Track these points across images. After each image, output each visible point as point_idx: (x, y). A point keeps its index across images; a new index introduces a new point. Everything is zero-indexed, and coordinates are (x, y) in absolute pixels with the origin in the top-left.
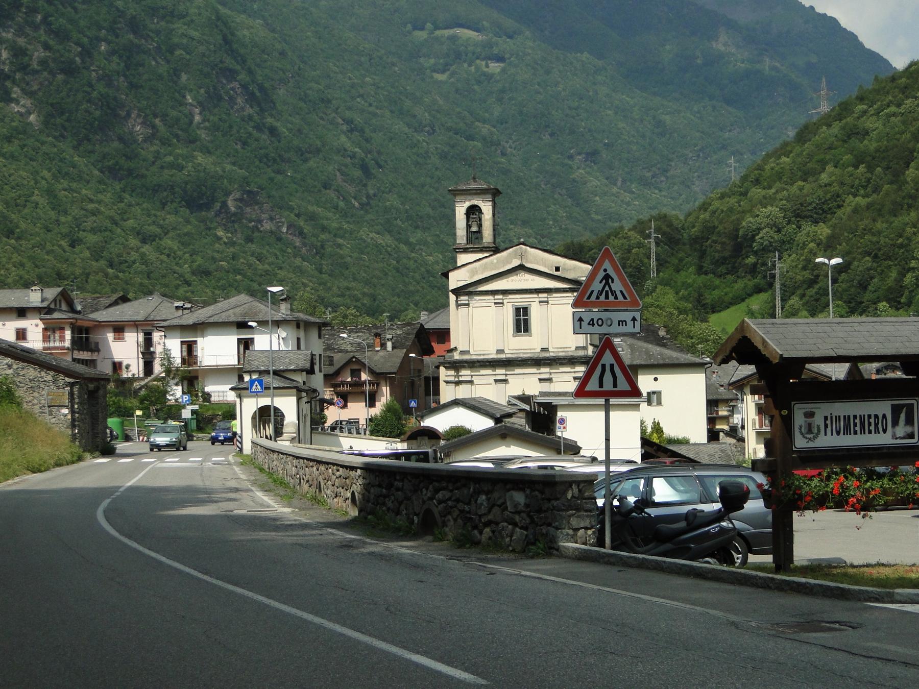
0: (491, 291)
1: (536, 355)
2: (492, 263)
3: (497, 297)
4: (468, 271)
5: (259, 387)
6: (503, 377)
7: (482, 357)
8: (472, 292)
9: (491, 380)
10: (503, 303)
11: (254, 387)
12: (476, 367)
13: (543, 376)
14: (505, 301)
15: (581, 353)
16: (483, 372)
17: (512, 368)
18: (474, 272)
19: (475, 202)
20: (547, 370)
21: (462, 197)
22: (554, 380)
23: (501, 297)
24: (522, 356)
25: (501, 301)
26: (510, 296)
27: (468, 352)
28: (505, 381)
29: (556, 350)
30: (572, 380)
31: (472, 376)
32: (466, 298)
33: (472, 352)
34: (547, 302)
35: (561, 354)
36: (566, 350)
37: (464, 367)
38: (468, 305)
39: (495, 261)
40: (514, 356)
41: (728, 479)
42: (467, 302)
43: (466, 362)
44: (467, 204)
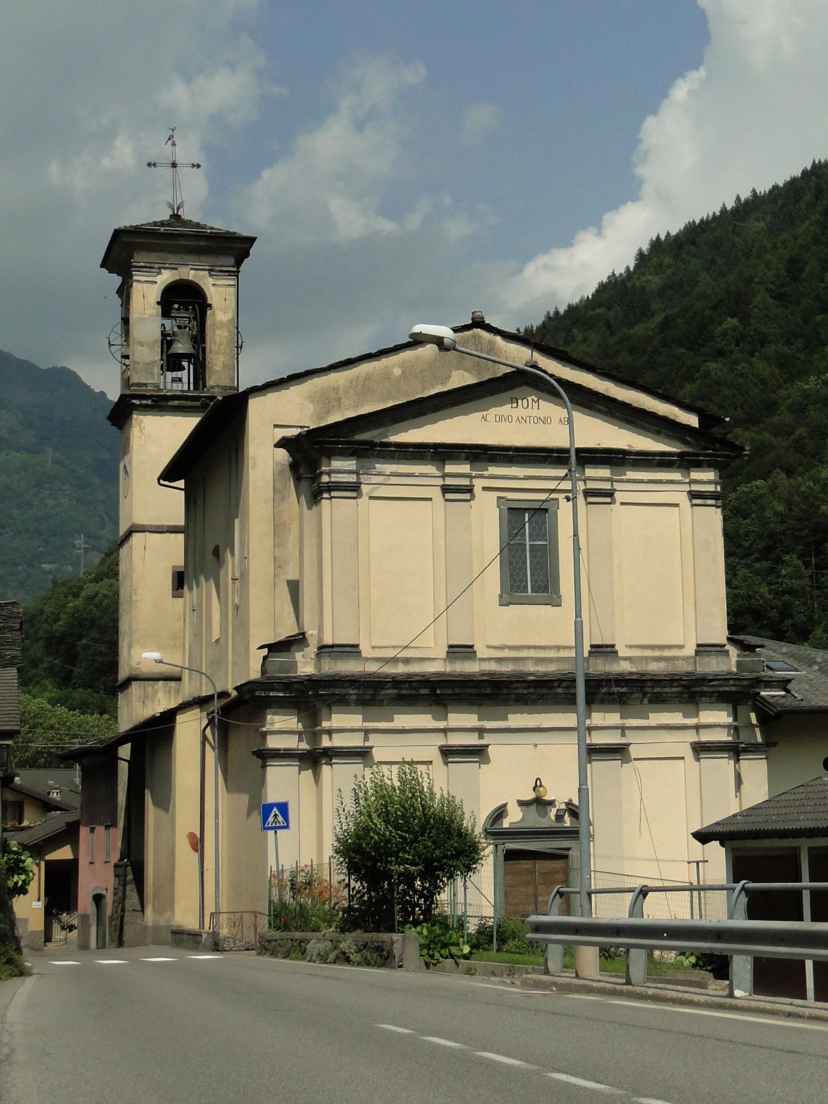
0: (436, 446)
1: (684, 667)
2: (387, 374)
3: (450, 468)
4: (311, 398)
5: (280, 818)
6: (472, 740)
7: (400, 669)
8: (371, 444)
9: (681, 743)
10: (469, 490)
11: (271, 819)
12: (380, 703)
13: (456, 740)
14: (479, 484)
15: (714, 666)
16: (403, 720)
17: (502, 709)
18: (327, 400)
19: (191, 275)
20: (470, 719)
21: (153, 257)
22: (634, 751)
23: (465, 468)
24: (531, 668)
25: (465, 482)
26: (493, 470)
27: (351, 650)
28: (478, 753)
29: (637, 653)
30: (689, 753)
31: (367, 732)
32: (350, 464)
33: (366, 651)
34: (610, 494)
35: (655, 667)
36: (667, 653)
37: (341, 702)
38: (355, 488)
39: (397, 372)
40: (507, 668)
41: (611, 985)
42: (352, 478)
43: (354, 682)
44: (166, 277)
